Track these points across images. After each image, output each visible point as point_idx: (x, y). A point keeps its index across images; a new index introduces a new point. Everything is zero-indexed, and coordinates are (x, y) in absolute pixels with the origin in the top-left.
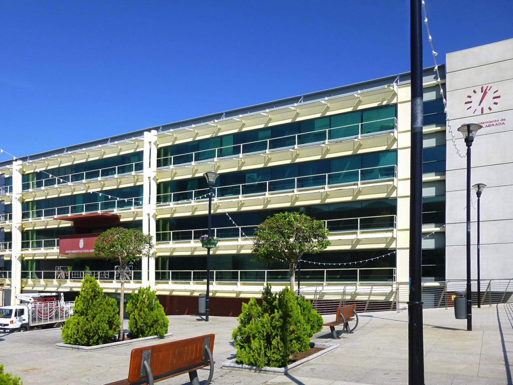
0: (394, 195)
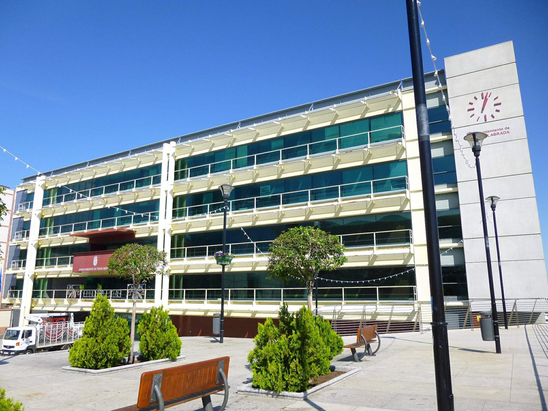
0: (407, 208)
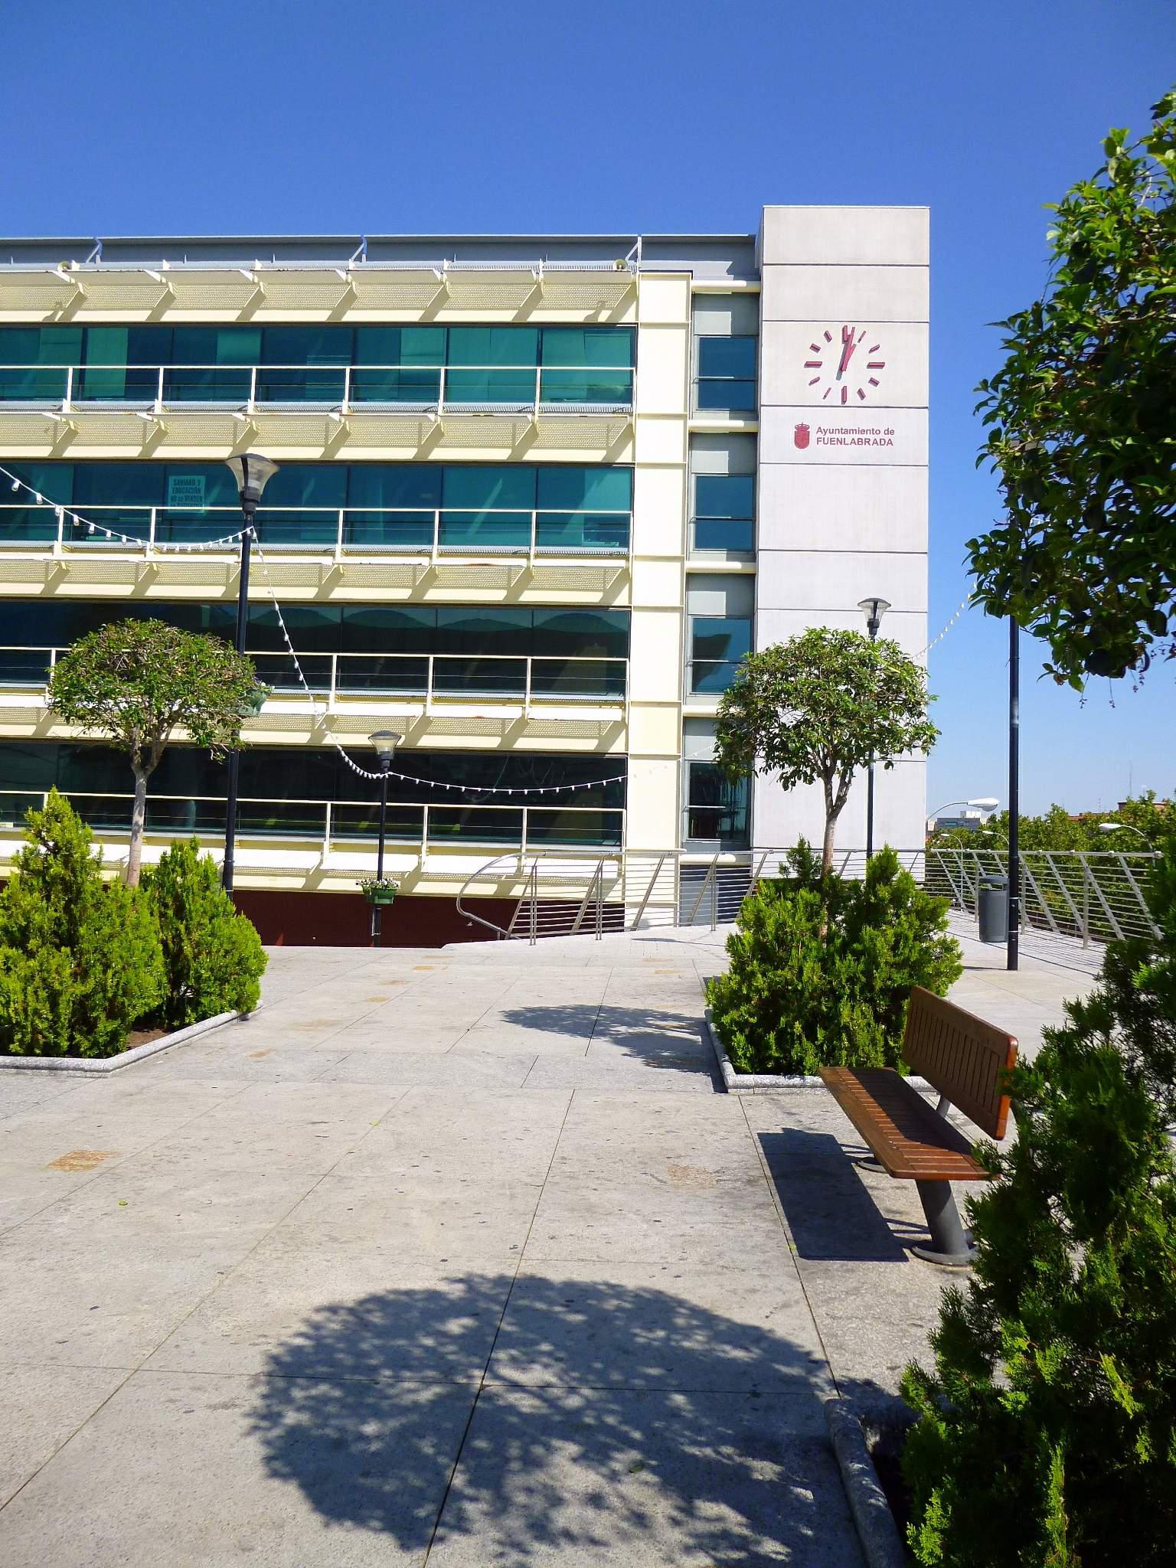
0: (621, 600)
